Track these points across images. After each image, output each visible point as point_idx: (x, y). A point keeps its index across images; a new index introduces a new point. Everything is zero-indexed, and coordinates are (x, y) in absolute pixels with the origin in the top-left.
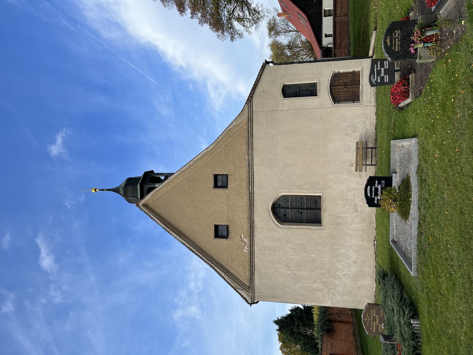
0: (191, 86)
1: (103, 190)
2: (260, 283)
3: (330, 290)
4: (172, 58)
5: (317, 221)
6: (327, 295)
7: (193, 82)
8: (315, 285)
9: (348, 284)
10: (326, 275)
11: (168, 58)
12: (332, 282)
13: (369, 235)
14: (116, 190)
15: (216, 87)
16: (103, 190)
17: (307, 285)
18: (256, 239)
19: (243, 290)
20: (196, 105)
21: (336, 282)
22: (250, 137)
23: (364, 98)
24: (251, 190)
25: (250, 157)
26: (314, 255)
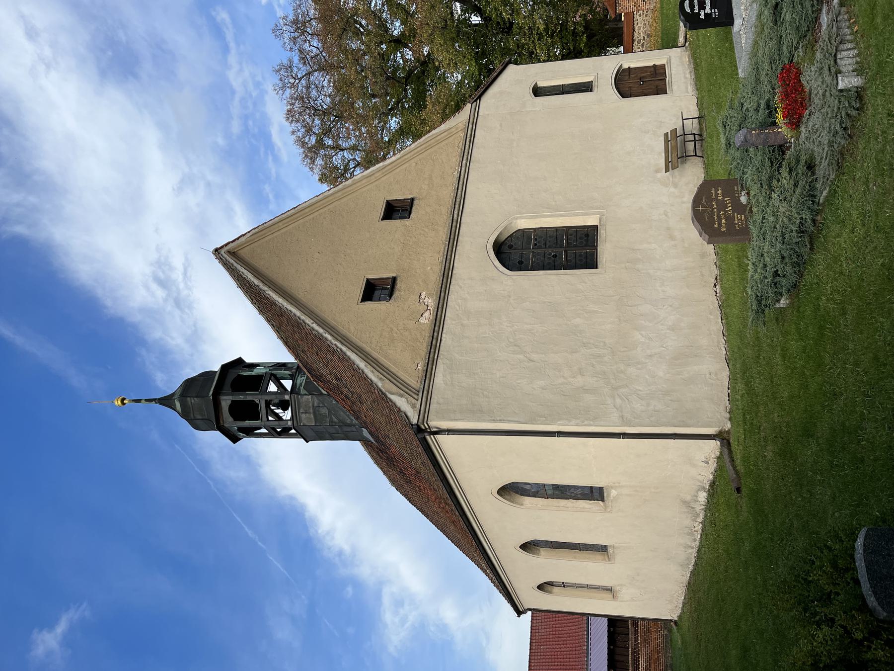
0: (350, 590)
1: (138, 401)
2: (446, 384)
3: (616, 389)
4: (328, 533)
5: (590, 262)
6: (609, 401)
7: (358, 584)
8: (579, 381)
9: (661, 374)
10: (606, 359)
11: (320, 531)
12: (622, 372)
13: (703, 275)
14: (167, 401)
15: (399, 603)
16: (138, 401)
17: (561, 380)
18: (452, 298)
19: (401, 396)
20: (351, 630)
21: (632, 370)
22: (468, 143)
23: (675, 88)
24: (455, 216)
25: (463, 169)
26: (578, 321)
